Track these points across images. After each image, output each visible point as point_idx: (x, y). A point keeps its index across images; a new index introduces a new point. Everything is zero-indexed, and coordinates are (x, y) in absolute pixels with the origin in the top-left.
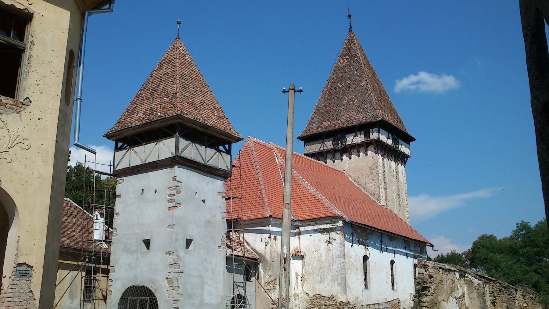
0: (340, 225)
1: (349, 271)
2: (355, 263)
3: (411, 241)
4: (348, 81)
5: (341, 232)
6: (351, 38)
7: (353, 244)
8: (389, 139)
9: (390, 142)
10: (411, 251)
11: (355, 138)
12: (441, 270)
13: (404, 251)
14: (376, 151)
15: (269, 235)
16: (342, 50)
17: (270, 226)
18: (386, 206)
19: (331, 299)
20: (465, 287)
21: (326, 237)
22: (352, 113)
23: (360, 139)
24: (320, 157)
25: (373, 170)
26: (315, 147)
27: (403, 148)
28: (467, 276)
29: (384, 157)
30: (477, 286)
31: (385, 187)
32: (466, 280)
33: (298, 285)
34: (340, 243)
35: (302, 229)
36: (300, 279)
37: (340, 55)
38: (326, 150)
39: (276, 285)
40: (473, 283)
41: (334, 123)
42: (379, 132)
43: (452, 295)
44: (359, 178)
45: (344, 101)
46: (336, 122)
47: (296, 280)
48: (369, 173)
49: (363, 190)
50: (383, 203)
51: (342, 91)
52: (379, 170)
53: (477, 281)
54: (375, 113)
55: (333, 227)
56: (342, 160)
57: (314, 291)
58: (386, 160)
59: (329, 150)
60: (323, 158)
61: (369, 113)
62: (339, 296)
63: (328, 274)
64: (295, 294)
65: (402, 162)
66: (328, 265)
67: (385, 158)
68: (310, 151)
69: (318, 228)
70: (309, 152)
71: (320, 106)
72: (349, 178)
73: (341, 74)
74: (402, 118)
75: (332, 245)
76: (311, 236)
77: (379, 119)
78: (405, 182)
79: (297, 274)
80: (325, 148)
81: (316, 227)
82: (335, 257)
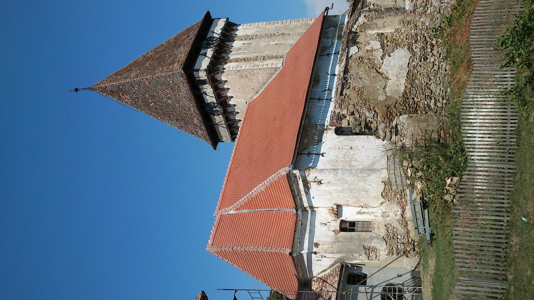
0: (299, 172)
1: (353, 163)
2: (343, 150)
3: (321, 46)
4: (147, 96)
5: (306, 172)
6: (100, 89)
7: (321, 152)
8: (206, 53)
9: (210, 52)
10: (333, 44)
11: (208, 94)
12: (344, 93)
13: (333, 56)
14: (220, 73)
15: (313, 254)
16: (115, 99)
17: (302, 252)
18: (283, 58)
19: (387, 183)
20: (370, 32)
21: (314, 187)
22: (180, 96)
23: (208, 89)
24: (234, 126)
25: (242, 75)
26: (224, 132)
27: (218, 29)
28: (355, 30)
29: (228, 59)
30: (368, 18)
31: (262, 58)
32: (360, 30)
33: (372, 213)
34: (320, 173)
35: (306, 205)
36: (364, 210)
37: (119, 101)
38: (226, 122)
39: (371, 247)
40: (364, 23)
41: (194, 114)
42: (198, 70)
43: (378, 66)
44: (253, 89)
45: (169, 102)
46: (193, 112)
47: (365, 214)
48: (247, 79)
49: (267, 85)
50: (279, 64)
51: (158, 103)
52: (242, 69)
53: (361, 19)
54: (177, 74)
55: (300, 178)
56: (235, 105)
57: (378, 198)
58: (232, 56)
59: (224, 118)
60: (235, 123)
61: (178, 80)
62: (383, 176)
63: (358, 185)
64: (382, 216)
65: (234, 30)
66: (347, 185)
67: (229, 58)
68: (228, 136)
69: (304, 191)
70: (229, 138)
71: (178, 125)
72: (254, 98)
73: (140, 102)
74: (185, 28)
75: (325, 153)
76: (313, 198)
77: (182, 71)
78: (257, 24)
79: (359, 213)
80: (223, 122)
81: (303, 193)
82: (337, 178)
